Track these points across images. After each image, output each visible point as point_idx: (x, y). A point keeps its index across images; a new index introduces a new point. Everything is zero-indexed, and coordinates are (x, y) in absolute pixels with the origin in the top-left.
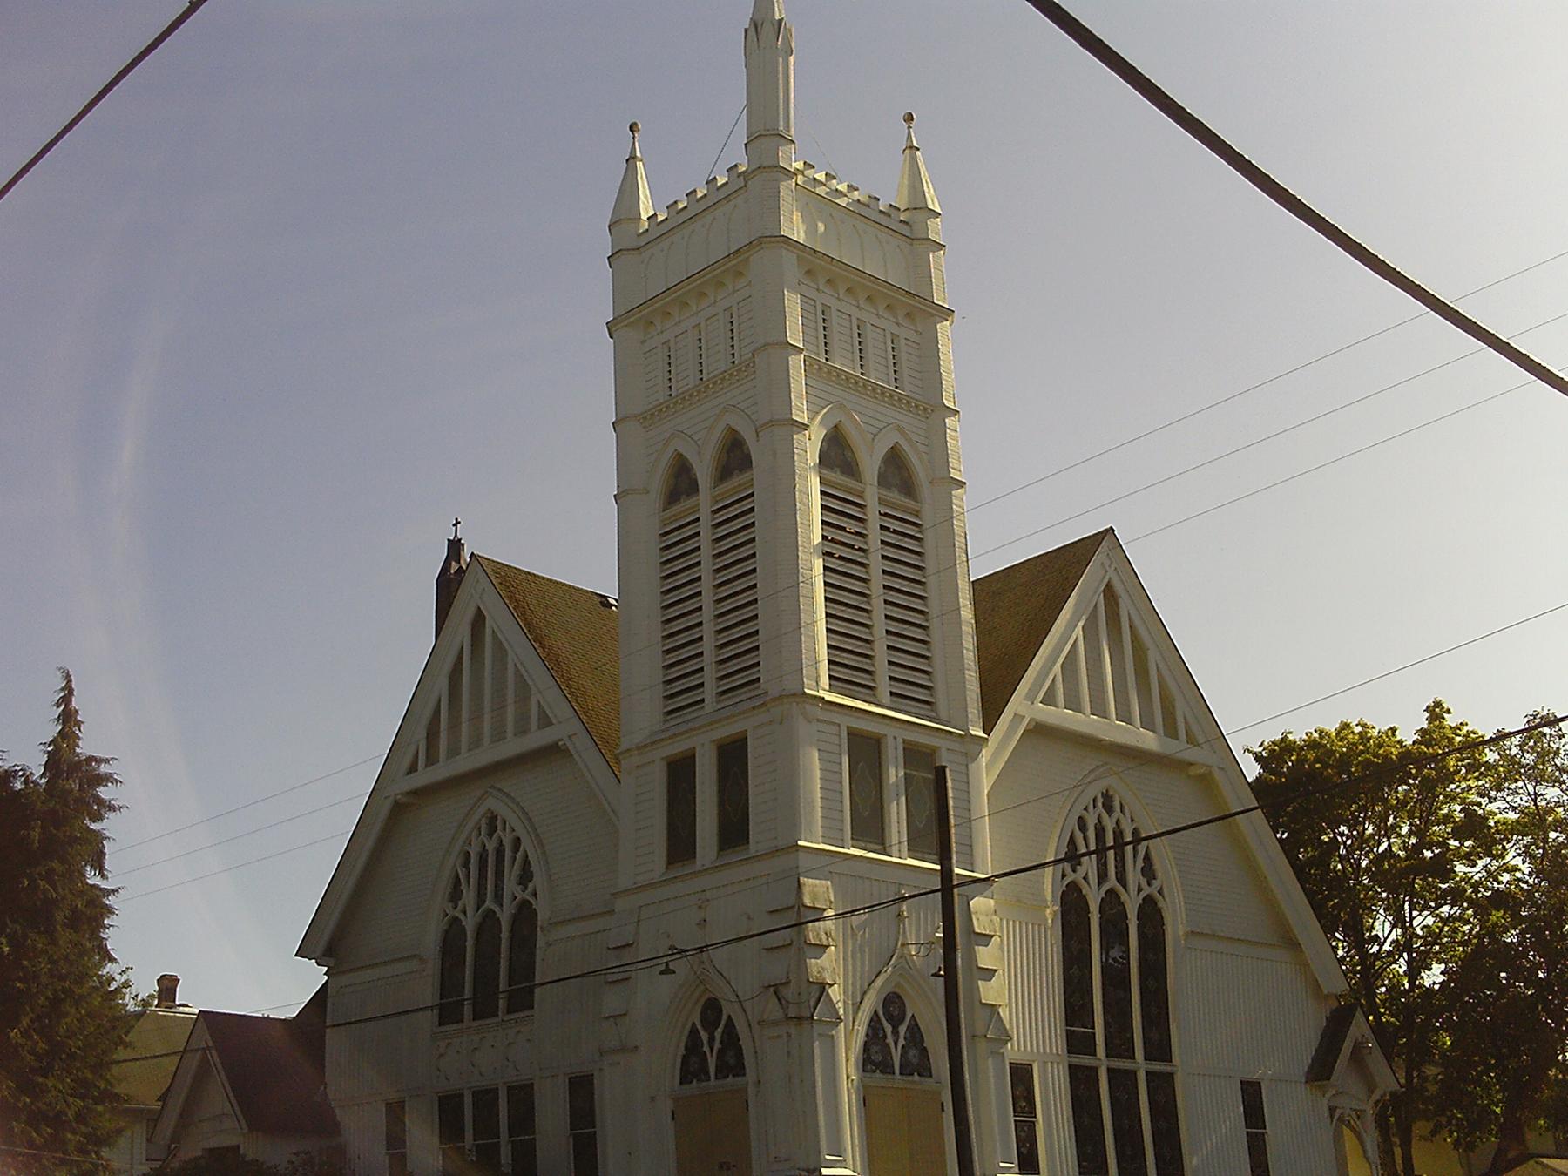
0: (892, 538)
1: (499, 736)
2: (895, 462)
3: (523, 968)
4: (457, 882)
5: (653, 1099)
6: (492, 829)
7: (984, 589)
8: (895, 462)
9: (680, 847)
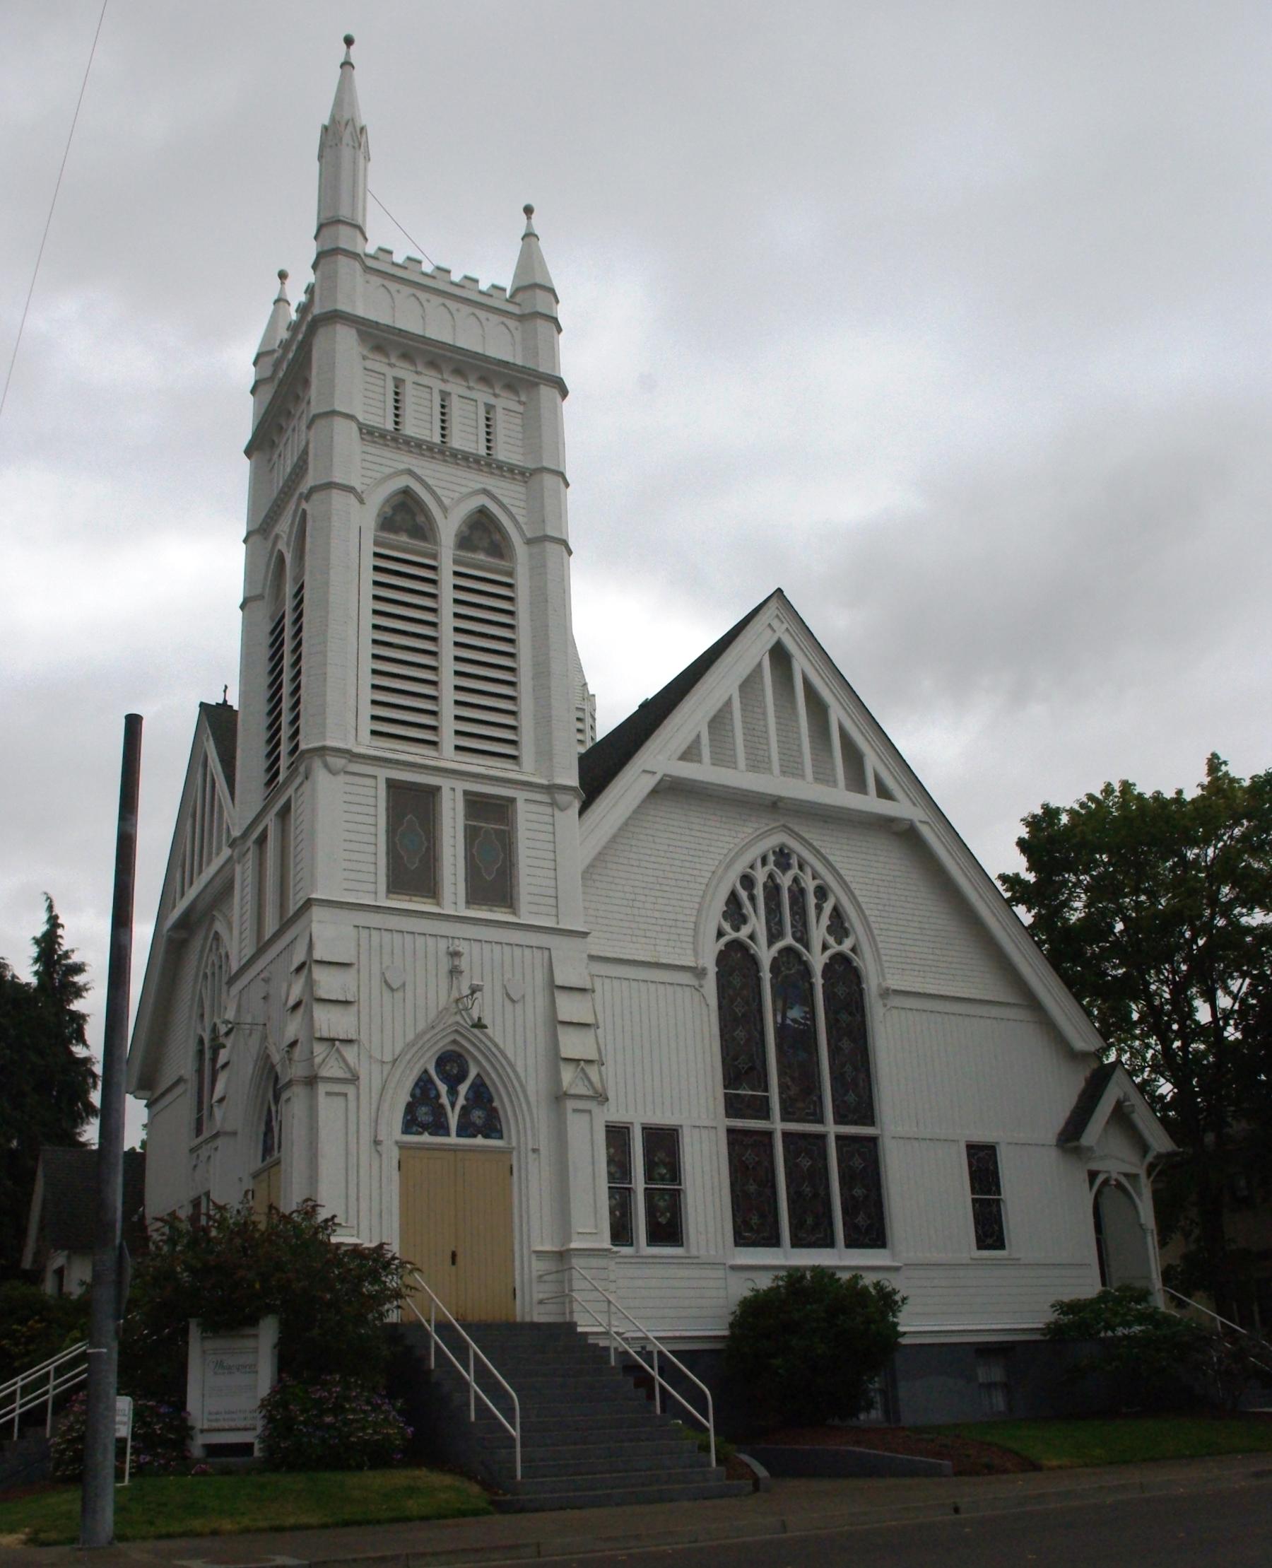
2: (483, 532)
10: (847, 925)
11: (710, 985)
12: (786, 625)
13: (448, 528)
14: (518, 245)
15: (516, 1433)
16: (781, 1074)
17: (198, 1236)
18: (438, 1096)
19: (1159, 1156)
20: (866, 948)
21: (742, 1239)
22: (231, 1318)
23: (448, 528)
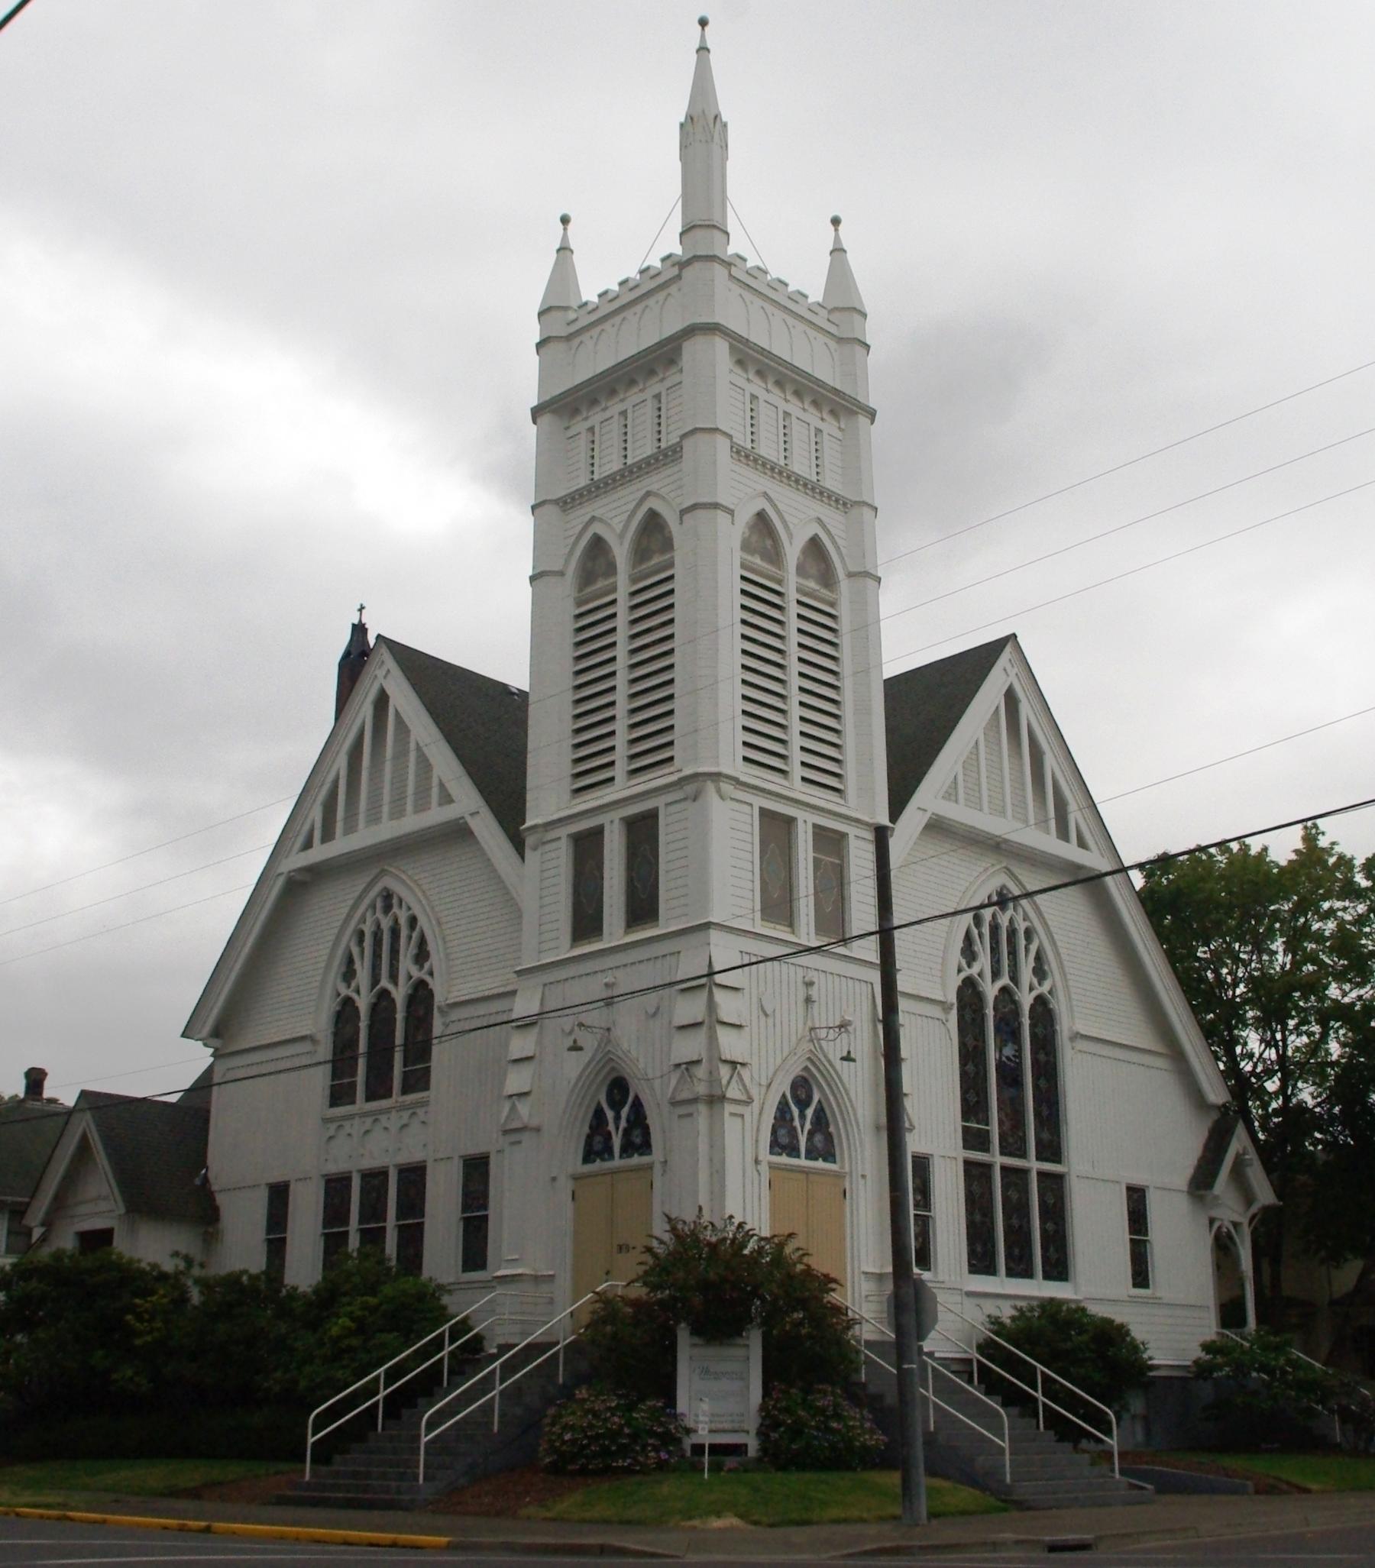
0: (780, 705)
1: (398, 813)
3: (420, 1050)
4: (350, 961)
5: (554, 1179)
6: (387, 908)
7: (894, 686)
8: (815, 547)
9: (586, 922)
10: (1046, 968)
11: (953, 1016)
12: (1016, 670)
13: (793, 552)
14: (827, 259)
15: (1006, 1445)
16: (1000, 1109)
17: (779, 1259)
18: (792, 1119)
19: (1266, 1209)
20: (1061, 993)
21: (974, 1269)
22: (719, 1325)
23: (793, 552)
